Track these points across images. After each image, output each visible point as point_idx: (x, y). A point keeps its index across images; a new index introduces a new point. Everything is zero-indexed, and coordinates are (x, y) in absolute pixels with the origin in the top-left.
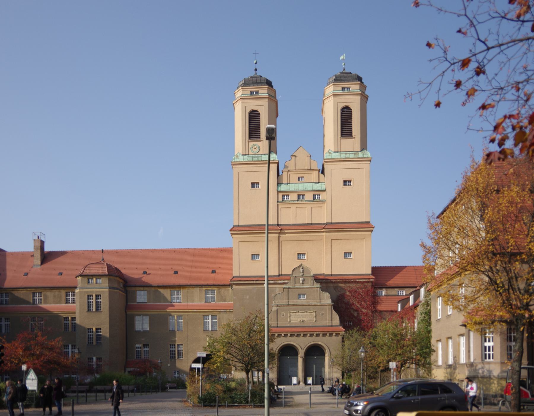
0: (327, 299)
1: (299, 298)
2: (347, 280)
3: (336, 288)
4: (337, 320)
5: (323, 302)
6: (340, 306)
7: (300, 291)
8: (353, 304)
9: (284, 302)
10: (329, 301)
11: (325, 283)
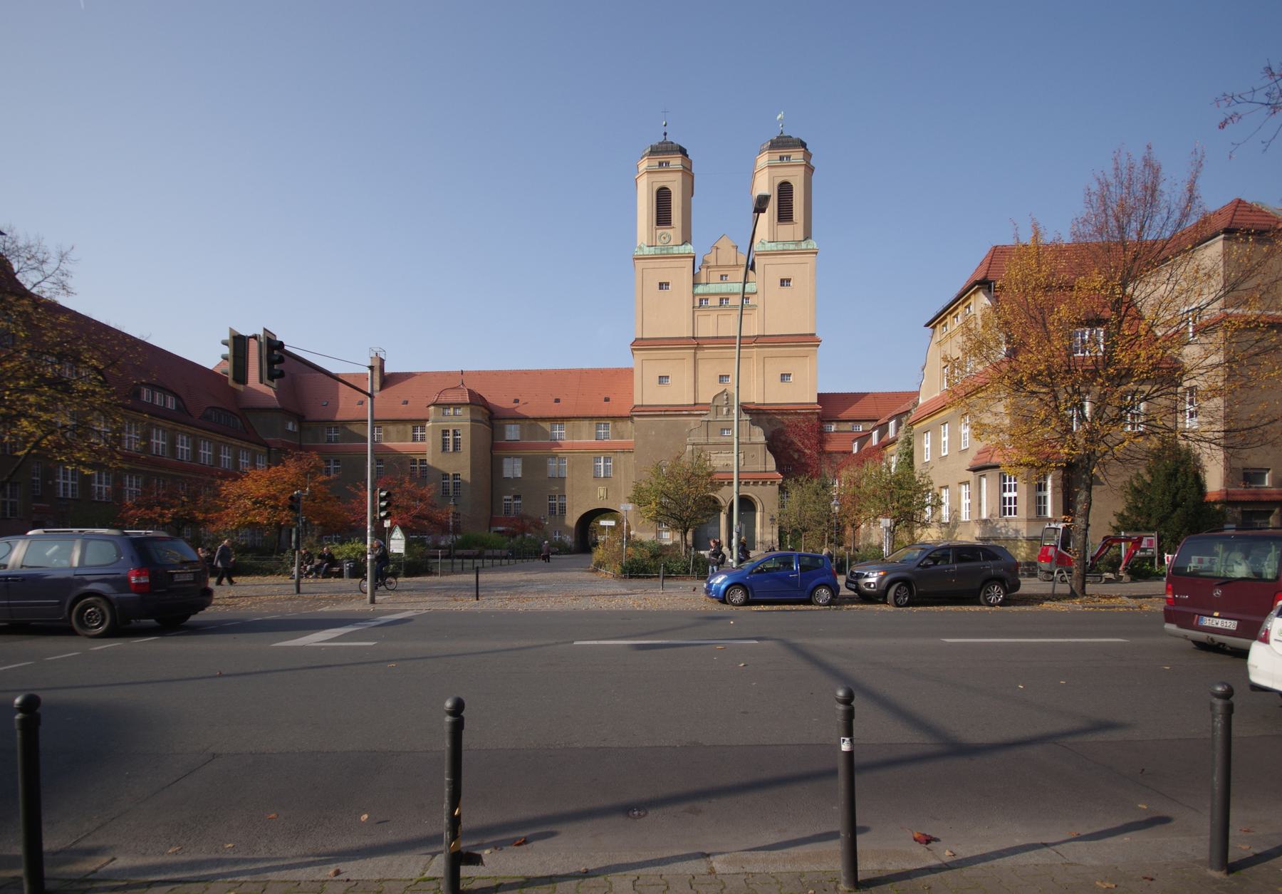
0: (759, 436)
1: (722, 434)
2: (783, 411)
3: (769, 421)
4: (772, 464)
5: (754, 439)
6: (776, 444)
7: (724, 425)
8: (792, 442)
9: (702, 440)
10: (762, 439)
11: (756, 414)
